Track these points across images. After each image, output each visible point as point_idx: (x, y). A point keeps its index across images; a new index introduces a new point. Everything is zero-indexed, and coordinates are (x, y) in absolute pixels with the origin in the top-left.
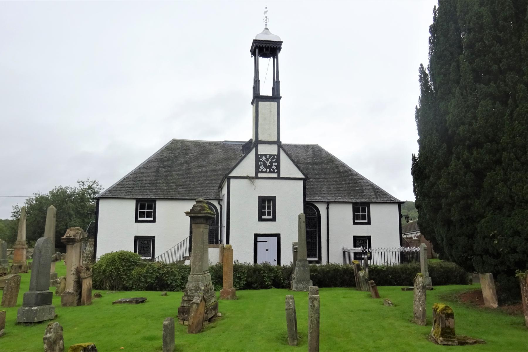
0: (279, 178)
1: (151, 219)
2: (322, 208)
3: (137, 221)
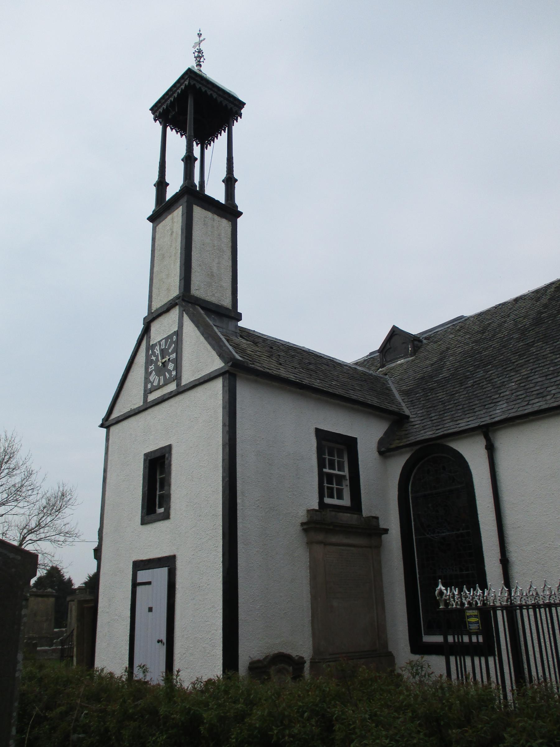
0: (181, 391)
2: (473, 453)
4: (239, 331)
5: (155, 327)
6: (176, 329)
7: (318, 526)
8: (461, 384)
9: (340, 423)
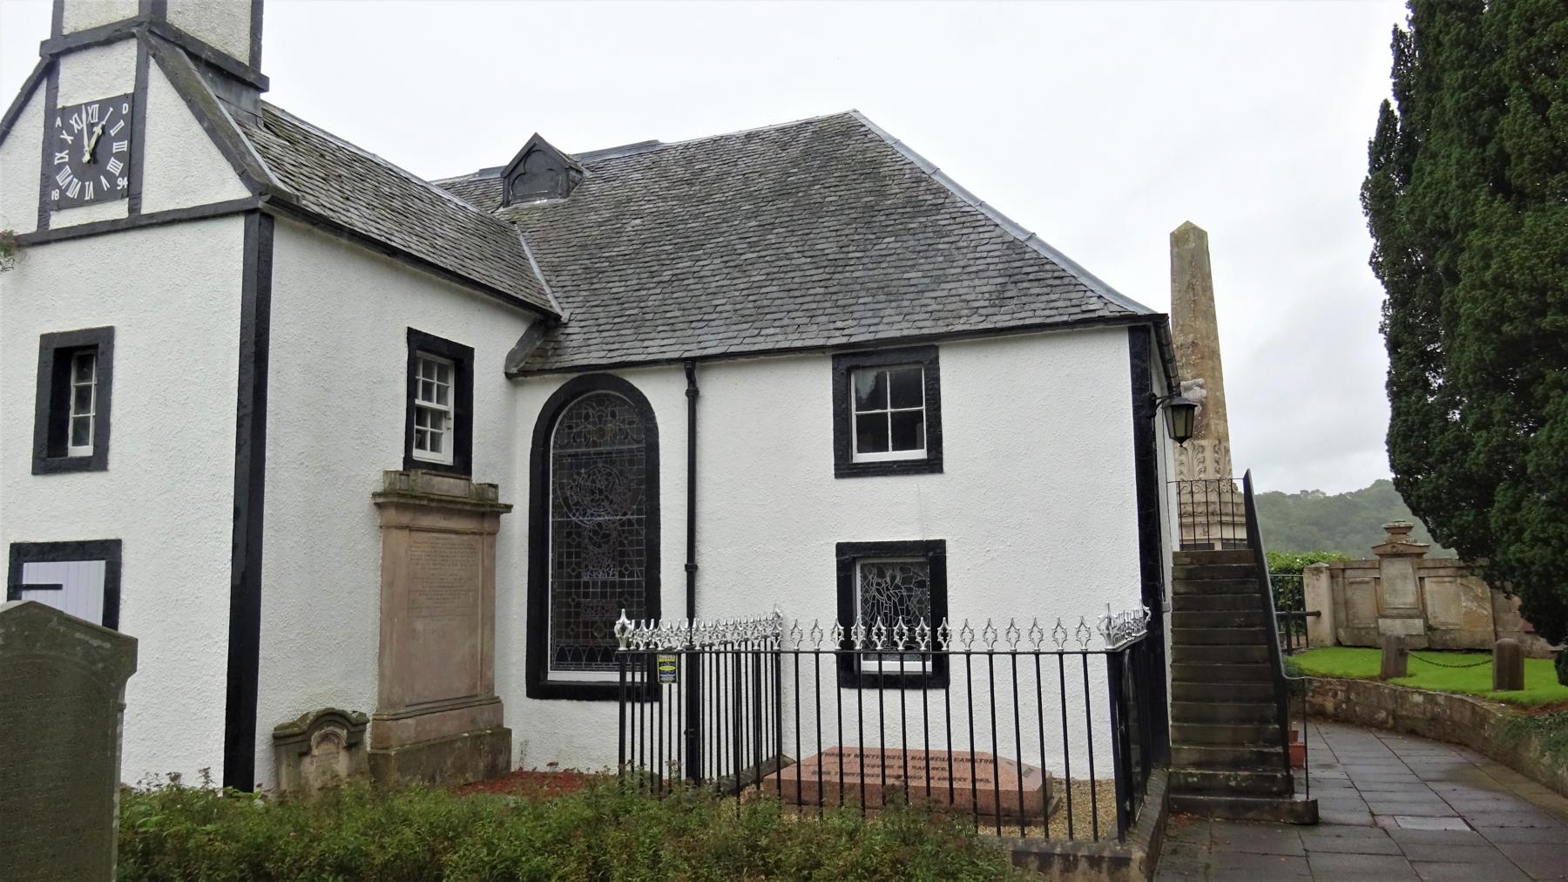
0: (138, 223)
1: (920, 454)
2: (665, 398)
3: (845, 468)
4: (260, 114)
5: (69, 69)
6: (130, 90)
7: (401, 500)
8: (652, 274)
9: (449, 321)
